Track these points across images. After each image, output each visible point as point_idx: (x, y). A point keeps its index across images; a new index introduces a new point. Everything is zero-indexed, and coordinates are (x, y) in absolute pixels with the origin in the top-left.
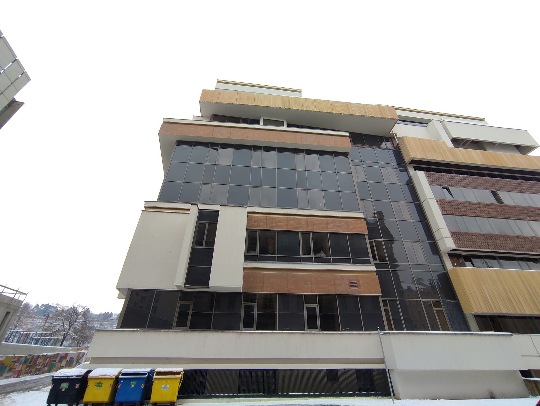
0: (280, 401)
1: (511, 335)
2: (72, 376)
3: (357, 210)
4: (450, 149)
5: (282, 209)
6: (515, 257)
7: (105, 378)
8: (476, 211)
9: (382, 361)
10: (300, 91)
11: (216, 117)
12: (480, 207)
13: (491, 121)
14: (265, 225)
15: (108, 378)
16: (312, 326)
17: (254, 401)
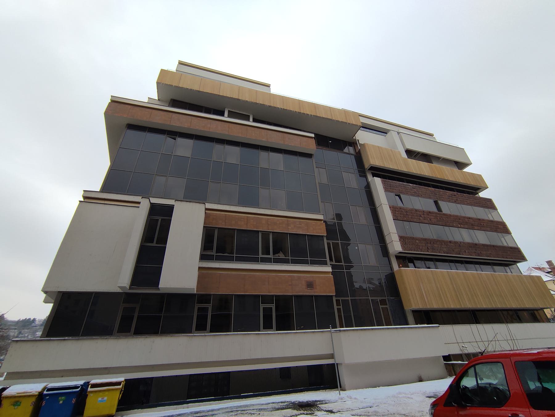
0: (231, 403)
1: (439, 326)
3: (318, 212)
4: (404, 159)
5: (242, 207)
8: (421, 218)
9: (332, 356)
11: (175, 103)
13: (440, 138)
14: (223, 223)
16: (268, 326)
17: (204, 405)
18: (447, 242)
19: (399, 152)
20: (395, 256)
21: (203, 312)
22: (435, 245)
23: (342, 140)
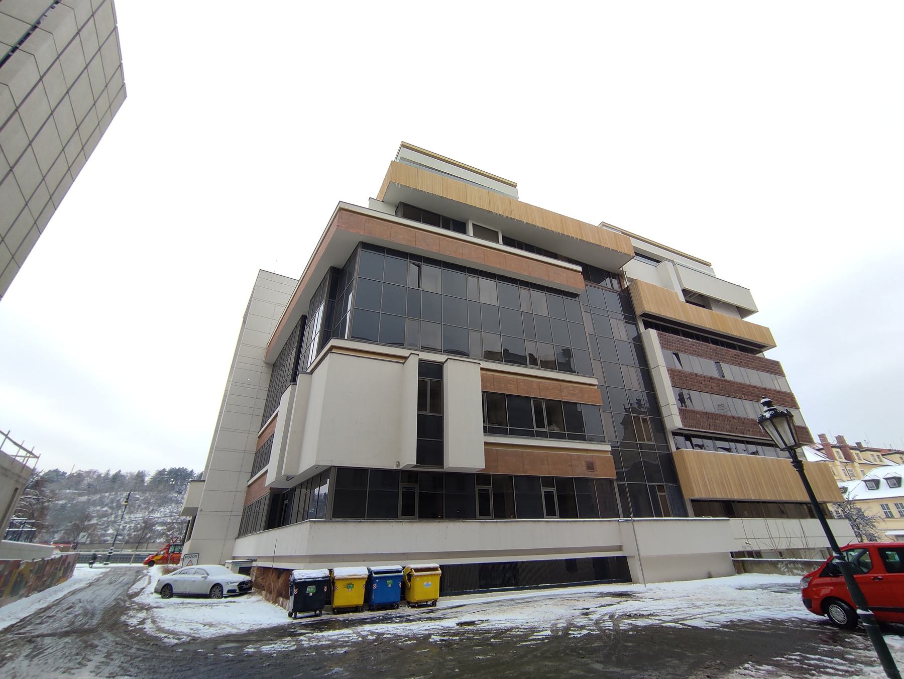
0: (531, 593)
1: (729, 520)
2: (318, 578)
3: (591, 375)
6: (727, 439)
7: (355, 579)
8: (702, 385)
9: (620, 548)
10: (513, 185)
12: (705, 380)
13: (721, 271)
14: (492, 387)
15: (359, 579)
16: (551, 513)
18: (730, 417)
19: (676, 293)
20: (672, 432)
21: (484, 496)
22: (718, 421)
23: (605, 271)
